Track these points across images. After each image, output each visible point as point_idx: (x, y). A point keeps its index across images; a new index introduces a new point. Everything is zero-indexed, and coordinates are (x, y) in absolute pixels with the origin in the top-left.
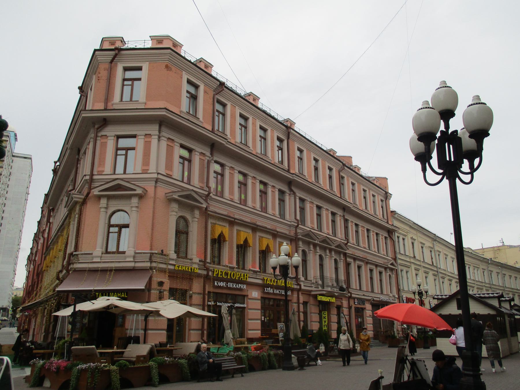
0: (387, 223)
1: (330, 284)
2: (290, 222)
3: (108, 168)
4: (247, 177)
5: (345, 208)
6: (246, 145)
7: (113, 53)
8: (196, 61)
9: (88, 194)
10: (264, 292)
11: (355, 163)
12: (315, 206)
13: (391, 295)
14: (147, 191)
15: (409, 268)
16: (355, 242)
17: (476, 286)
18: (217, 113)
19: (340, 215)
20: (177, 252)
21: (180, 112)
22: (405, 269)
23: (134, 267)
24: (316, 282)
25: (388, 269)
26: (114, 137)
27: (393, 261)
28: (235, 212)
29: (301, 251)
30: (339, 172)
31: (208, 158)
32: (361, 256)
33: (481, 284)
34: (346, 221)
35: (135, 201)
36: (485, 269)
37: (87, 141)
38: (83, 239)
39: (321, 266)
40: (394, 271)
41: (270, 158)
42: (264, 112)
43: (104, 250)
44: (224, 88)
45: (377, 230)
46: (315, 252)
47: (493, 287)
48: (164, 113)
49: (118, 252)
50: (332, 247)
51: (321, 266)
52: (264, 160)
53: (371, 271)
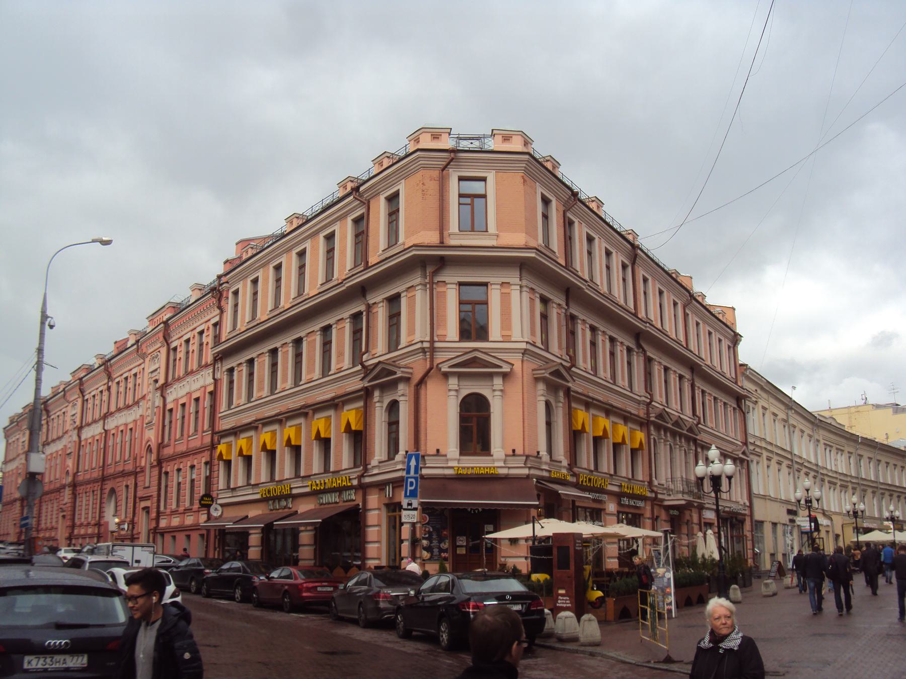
0: (736, 383)
2: (640, 396)
5: (570, 292)
10: (620, 504)
12: (538, 296)
17: (839, 483)
19: (688, 380)
22: (755, 458)
23: (508, 474)
25: (738, 461)
33: (834, 475)
34: (693, 386)
35: (498, 382)
36: (852, 453)
45: (716, 393)
47: (862, 483)
48: (533, 255)
52: (609, 299)
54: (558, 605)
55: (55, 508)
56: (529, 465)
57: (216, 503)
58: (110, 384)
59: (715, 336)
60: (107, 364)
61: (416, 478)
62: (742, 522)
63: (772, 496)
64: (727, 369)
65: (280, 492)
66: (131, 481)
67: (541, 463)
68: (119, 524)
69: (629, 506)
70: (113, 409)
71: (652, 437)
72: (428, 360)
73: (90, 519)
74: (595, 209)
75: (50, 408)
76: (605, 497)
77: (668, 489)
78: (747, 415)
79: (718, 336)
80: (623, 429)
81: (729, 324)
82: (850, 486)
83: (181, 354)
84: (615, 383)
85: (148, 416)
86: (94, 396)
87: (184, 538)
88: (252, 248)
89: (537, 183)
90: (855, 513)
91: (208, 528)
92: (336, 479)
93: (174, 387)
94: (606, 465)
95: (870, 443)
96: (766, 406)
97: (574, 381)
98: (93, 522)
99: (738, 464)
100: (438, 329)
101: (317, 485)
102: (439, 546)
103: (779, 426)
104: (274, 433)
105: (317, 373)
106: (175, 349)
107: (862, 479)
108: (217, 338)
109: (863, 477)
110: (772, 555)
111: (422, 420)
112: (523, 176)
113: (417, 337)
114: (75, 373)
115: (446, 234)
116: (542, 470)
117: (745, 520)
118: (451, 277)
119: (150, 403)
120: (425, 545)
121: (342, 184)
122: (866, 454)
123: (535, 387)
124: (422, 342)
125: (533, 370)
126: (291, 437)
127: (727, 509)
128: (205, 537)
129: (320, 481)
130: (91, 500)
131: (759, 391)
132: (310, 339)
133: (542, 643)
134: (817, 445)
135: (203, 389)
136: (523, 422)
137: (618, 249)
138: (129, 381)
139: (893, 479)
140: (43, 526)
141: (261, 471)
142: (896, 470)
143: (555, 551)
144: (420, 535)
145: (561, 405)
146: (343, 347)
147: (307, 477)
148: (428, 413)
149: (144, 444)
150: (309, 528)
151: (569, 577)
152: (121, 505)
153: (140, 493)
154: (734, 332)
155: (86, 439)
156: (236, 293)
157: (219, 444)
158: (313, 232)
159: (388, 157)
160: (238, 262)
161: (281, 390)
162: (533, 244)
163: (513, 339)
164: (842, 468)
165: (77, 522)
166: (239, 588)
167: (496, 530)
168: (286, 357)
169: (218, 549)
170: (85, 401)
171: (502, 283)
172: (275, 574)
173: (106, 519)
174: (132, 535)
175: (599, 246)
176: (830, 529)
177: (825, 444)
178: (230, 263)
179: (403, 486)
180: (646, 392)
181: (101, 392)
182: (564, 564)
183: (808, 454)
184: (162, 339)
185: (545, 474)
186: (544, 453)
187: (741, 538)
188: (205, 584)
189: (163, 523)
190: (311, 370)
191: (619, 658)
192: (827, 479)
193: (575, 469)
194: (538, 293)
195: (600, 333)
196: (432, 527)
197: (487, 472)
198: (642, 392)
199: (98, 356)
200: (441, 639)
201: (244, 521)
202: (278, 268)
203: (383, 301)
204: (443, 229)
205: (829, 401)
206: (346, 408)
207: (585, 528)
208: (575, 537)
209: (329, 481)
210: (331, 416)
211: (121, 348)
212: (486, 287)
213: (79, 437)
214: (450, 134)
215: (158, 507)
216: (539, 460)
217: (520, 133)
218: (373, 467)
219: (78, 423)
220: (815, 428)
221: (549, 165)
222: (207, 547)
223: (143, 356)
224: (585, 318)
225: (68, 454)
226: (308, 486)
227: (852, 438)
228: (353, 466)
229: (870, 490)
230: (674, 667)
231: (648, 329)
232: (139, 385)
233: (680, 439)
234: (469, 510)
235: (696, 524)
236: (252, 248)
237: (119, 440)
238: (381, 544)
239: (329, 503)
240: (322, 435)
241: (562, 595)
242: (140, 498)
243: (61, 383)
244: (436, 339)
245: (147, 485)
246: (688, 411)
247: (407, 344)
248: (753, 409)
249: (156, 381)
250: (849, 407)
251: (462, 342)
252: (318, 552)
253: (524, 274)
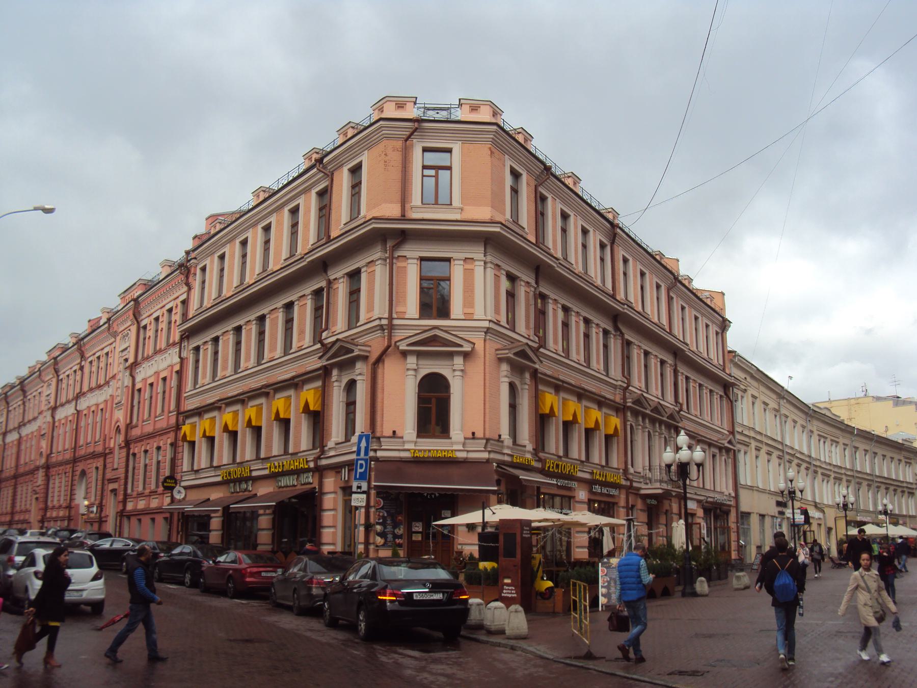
0: (724, 370)
2: (617, 381)
4: (569, 313)
5: (540, 270)
10: (591, 492)
12: (504, 273)
15: (748, 446)
17: (833, 475)
19: (670, 365)
22: (743, 448)
23: (467, 458)
25: (724, 451)
33: (828, 467)
34: (676, 372)
35: (458, 361)
45: (701, 380)
47: (858, 475)
48: (498, 230)
54: (503, 595)
55: (30, 490)
56: (489, 449)
57: (180, 486)
58: (83, 363)
59: (702, 321)
60: (80, 343)
61: (366, 460)
62: (727, 513)
63: (761, 487)
64: (715, 356)
65: (240, 474)
66: (100, 463)
67: (502, 447)
68: (88, 507)
69: (601, 494)
70: (85, 389)
71: (629, 423)
72: (386, 338)
73: (62, 502)
74: (571, 186)
75: (26, 389)
76: (574, 484)
77: (644, 477)
78: (734, 403)
79: (706, 321)
80: (596, 414)
81: (717, 309)
82: (844, 478)
83: (150, 333)
84: (589, 367)
85: (118, 396)
86: (68, 376)
87: (149, 521)
88: (220, 223)
89: (506, 156)
90: (845, 506)
91: (171, 511)
92: (294, 461)
93: (143, 366)
94: (577, 450)
95: (866, 436)
96: (756, 394)
97: (541, 362)
98: (64, 505)
99: (724, 454)
100: (397, 305)
101: (275, 467)
102: (394, 532)
103: (769, 416)
104: (236, 413)
105: (279, 351)
106: (145, 327)
107: (857, 471)
108: (185, 314)
109: (859, 469)
110: (759, 547)
111: (379, 400)
112: (490, 148)
113: (376, 314)
114: (51, 353)
115: (407, 206)
116: (504, 454)
117: (730, 511)
118: (412, 252)
119: (120, 383)
120: (379, 531)
121: (307, 156)
122: (862, 446)
123: (499, 367)
124: (380, 319)
125: (497, 350)
126: (252, 417)
127: (709, 500)
128: (169, 520)
129: (279, 464)
130: (63, 481)
131: (749, 379)
132: (273, 316)
133: (468, 635)
134: (811, 436)
135: (170, 368)
136: (484, 404)
137: (596, 228)
138: (101, 360)
139: (897, 474)
140: (18, 508)
141: (223, 454)
142: (893, 463)
143: (501, 538)
144: (375, 518)
145: (527, 387)
146: (305, 324)
147: (267, 459)
148: (385, 393)
149: (113, 425)
150: (268, 511)
151: (515, 566)
152: (91, 487)
153: (109, 475)
154: (723, 318)
155: (60, 420)
156: (204, 269)
157: (184, 425)
158: (278, 206)
159: (353, 128)
160: (206, 237)
161: (244, 369)
162: (499, 218)
163: (475, 317)
164: (909, 478)
165: (50, 504)
166: (189, 572)
167: (454, 515)
168: (250, 334)
169: (181, 533)
170: (59, 381)
171: (466, 258)
172: (221, 559)
173: (76, 502)
174: (101, 518)
175: (575, 224)
176: (822, 522)
177: (819, 435)
178: (199, 238)
179: (353, 469)
180: (623, 376)
181: (75, 371)
182: (510, 553)
183: (801, 445)
184: (132, 317)
185: (507, 458)
186: (506, 436)
187: (726, 530)
188: (157, 569)
189: (130, 506)
190: (273, 348)
191: (538, 652)
192: (820, 471)
193: (541, 455)
194: (504, 270)
195: (573, 313)
196: (387, 511)
197: (445, 455)
198: (619, 376)
199: (72, 335)
200: (360, 628)
201: (203, 504)
202: (244, 243)
203: (344, 277)
204: (404, 202)
205: (829, 392)
206: (306, 387)
207: (537, 515)
208: (525, 524)
209: (289, 464)
210: (291, 396)
211: (95, 327)
212: (448, 263)
213: (53, 417)
214: (415, 103)
215: (126, 489)
216: (500, 444)
217: (489, 103)
218: (330, 449)
219: (52, 404)
220: (809, 419)
221: (520, 138)
222: (170, 530)
223: (115, 335)
224: (556, 298)
225: (42, 435)
226: (267, 468)
227: (847, 430)
228: (311, 448)
229: (865, 483)
230: (590, 664)
231: (625, 311)
232: (110, 364)
233: (660, 426)
234: (425, 494)
235: (676, 514)
236: (220, 223)
237: (90, 421)
238: (336, 529)
239: (287, 486)
240: (282, 416)
241: (508, 585)
242: (108, 480)
243: (38, 362)
244: (395, 316)
245: (115, 466)
246: (670, 397)
247: (366, 321)
248: (742, 397)
249: (126, 360)
250: (849, 399)
251: (422, 319)
252: (276, 537)
253: (489, 250)
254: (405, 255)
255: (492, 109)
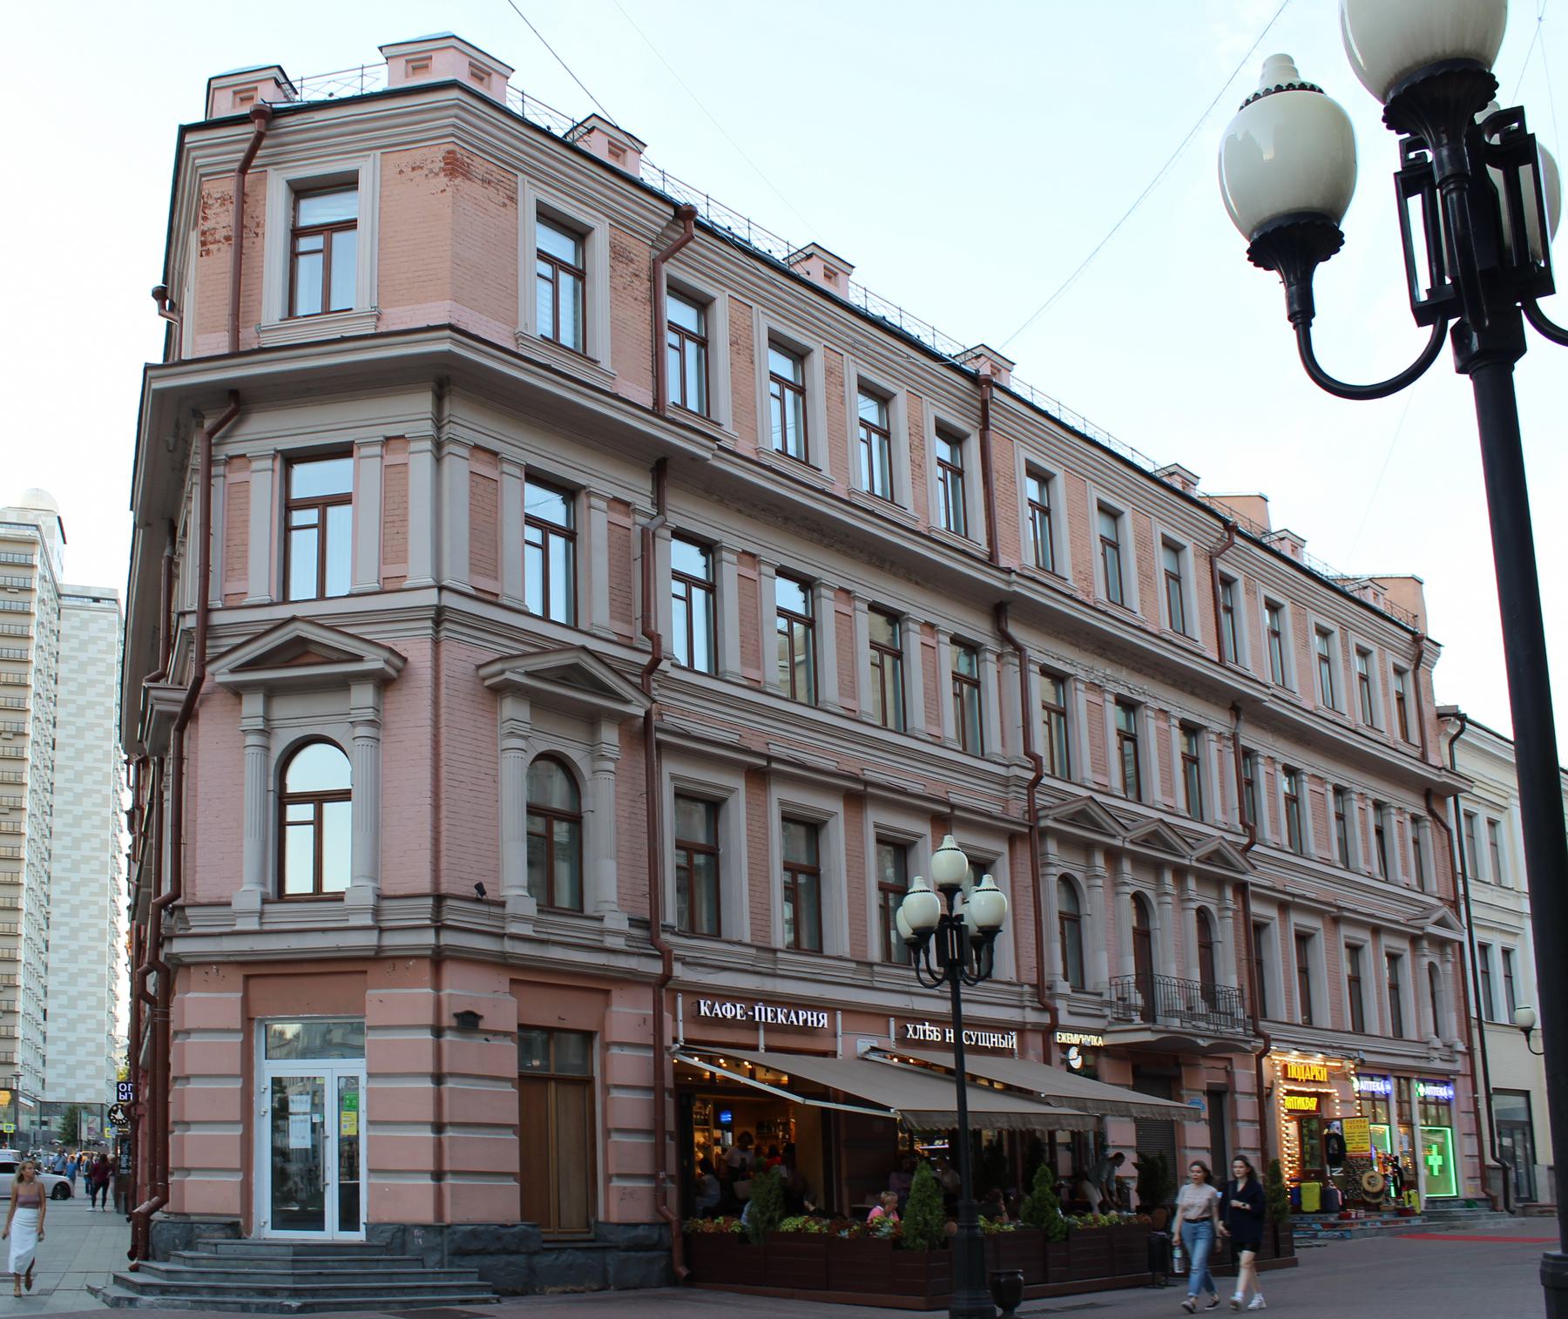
0: (1423, 758)
1: (1181, 1005)
2: (1008, 766)
3: (259, 583)
5: (1240, 706)
6: (806, 463)
7: (249, 130)
8: (574, 129)
9: (199, 681)
11: (1278, 520)
13: (1437, 1043)
14: (405, 660)
16: (1285, 841)
18: (672, 338)
20: (544, 885)
21: (517, 340)
24: (1119, 999)
25: (1425, 944)
26: (274, 458)
27: (1445, 911)
28: (865, 760)
29: (1055, 879)
30: (1210, 557)
31: (644, 521)
32: (1308, 895)
35: (363, 696)
37: (187, 487)
38: (195, 851)
39: (1143, 937)
40: (1449, 950)
41: (911, 511)
42: (879, 324)
43: (270, 889)
44: (696, 232)
46: (1117, 884)
49: (318, 894)
50: (1186, 862)
51: (1143, 937)
53: (1354, 950)
97: (1254, 867)
163: (407, 584)
221: (597, 146)
254: (241, 452)
255: (606, 139)
